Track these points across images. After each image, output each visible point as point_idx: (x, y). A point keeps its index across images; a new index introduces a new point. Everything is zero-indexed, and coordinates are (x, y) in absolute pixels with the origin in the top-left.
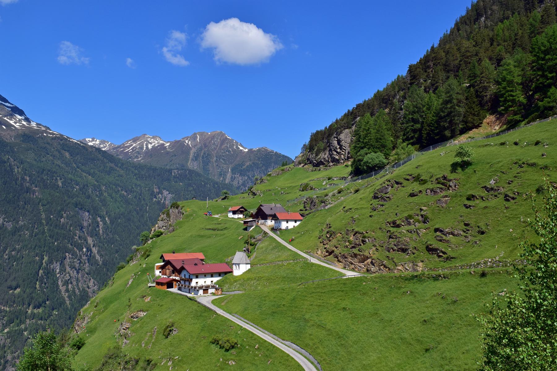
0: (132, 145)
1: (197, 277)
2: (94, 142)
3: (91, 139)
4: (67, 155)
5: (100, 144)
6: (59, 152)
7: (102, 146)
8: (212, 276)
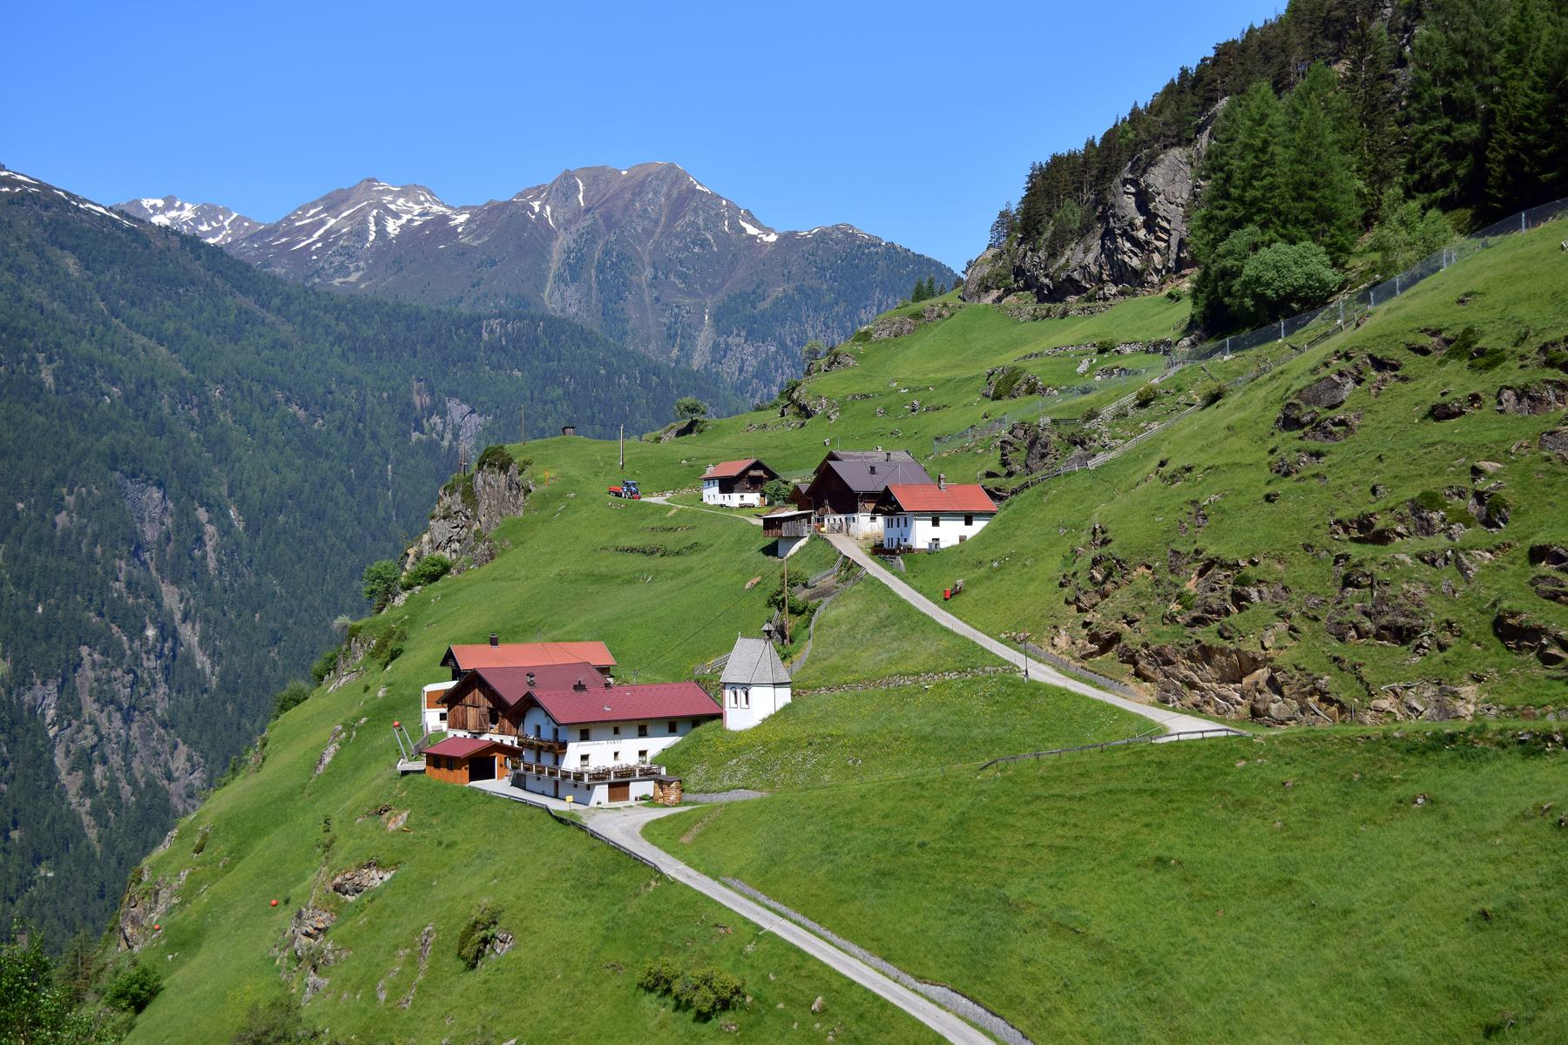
0: (322, 223)
1: (585, 736)
2: (173, 214)
3: (160, 203)
4: (71, 264)
5: (197, 221)
6: (40, 254)
7: (205, 228)
8: (643, 733)
